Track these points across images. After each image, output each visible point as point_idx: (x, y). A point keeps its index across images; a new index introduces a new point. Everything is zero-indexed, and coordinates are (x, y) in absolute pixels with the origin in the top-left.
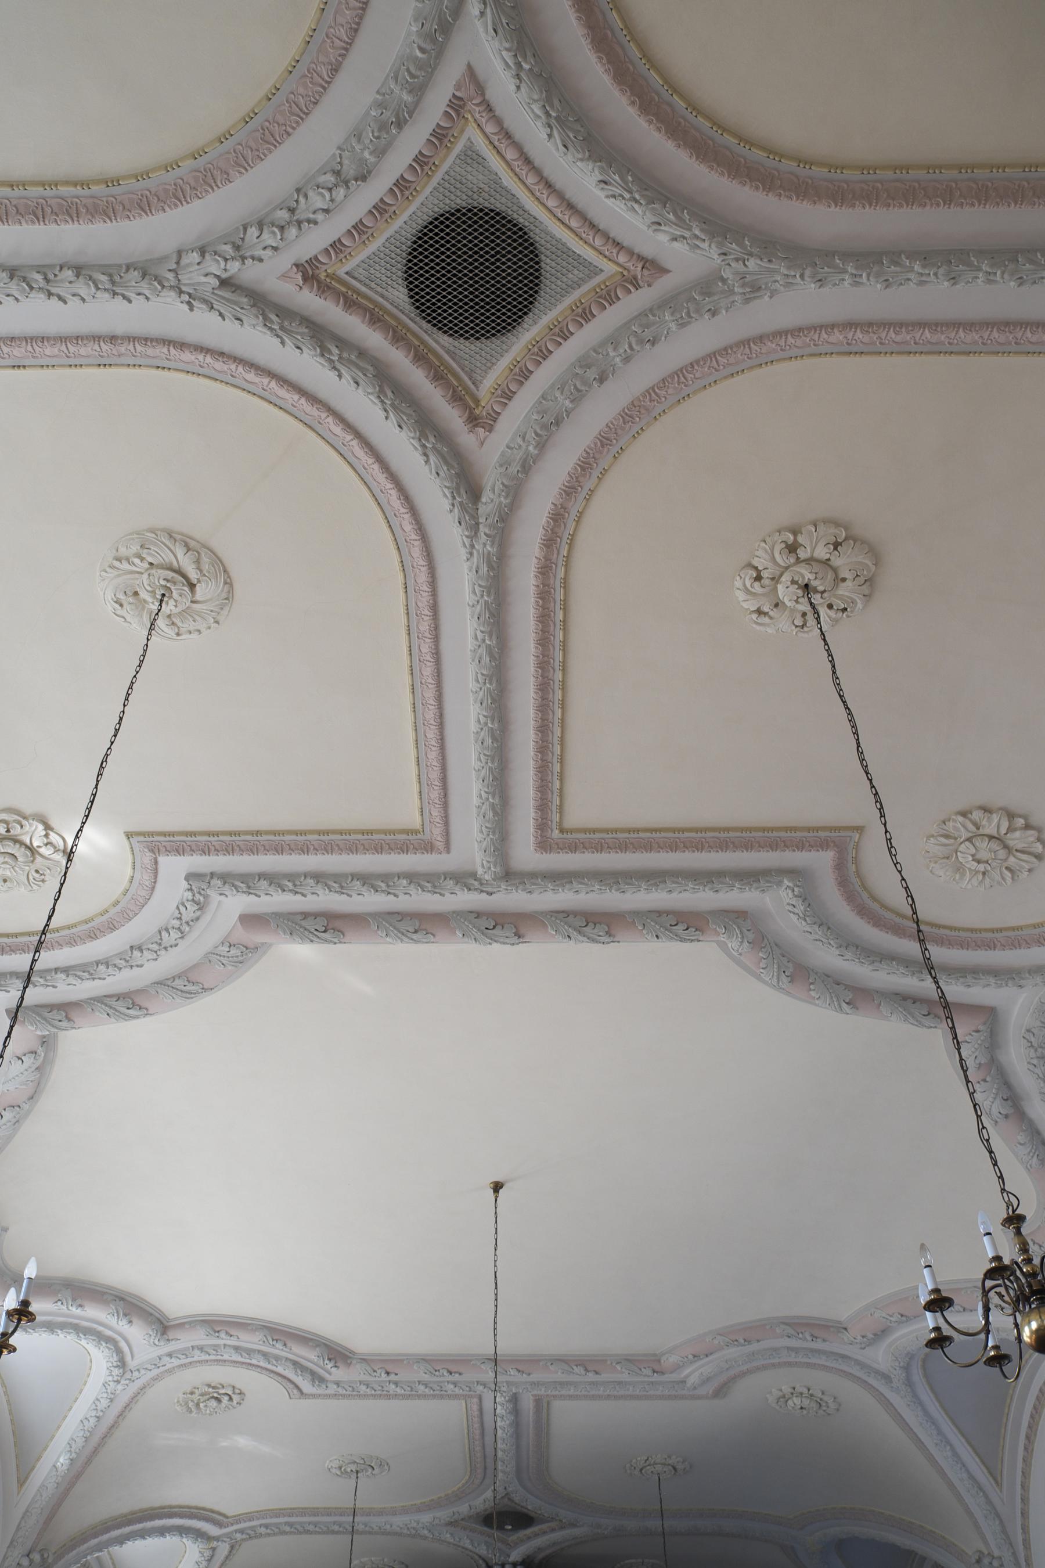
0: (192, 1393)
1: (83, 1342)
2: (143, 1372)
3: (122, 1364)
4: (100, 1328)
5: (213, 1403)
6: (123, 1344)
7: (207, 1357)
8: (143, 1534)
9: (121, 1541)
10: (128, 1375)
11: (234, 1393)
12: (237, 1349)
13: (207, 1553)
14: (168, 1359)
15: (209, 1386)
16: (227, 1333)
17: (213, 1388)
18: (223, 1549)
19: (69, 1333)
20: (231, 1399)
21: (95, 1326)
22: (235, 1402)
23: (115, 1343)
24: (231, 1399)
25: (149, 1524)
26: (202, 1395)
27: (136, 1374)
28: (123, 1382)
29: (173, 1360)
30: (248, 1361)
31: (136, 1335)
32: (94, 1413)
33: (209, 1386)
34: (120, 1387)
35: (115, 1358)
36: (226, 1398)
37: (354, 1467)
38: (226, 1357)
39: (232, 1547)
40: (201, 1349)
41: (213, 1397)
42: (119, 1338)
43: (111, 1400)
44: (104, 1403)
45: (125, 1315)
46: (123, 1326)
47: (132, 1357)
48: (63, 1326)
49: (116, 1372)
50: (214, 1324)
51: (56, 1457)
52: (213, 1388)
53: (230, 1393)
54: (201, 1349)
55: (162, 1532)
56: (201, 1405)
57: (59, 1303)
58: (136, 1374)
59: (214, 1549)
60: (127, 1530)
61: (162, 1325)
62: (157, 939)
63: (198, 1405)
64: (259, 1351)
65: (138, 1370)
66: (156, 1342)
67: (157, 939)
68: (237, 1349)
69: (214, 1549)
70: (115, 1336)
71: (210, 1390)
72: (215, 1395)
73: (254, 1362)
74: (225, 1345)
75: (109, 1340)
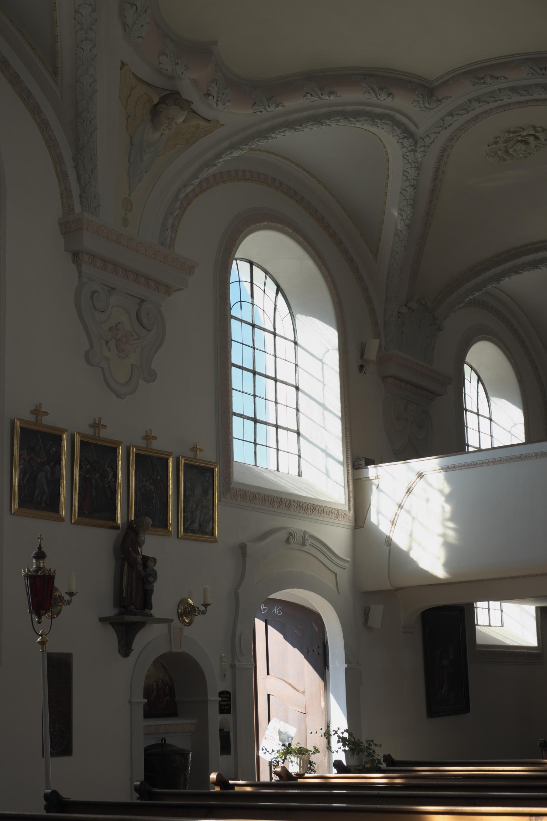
0: (496, 143)
1: (358, 125)
2: (433, 136)
3: (407, 134)
4: (368, 108)
6: (399, 117)
7: (486, 107)
8: (517, 270)
9: (497, 278)
11: (536, 131)
12: (513, 89)
14: (450, 118)
15: (509, 132)
16: (492, 77)
17: (514, 132)
19: (339, 120)
20: (537, 138)
21: (362, 108)
22: (543, 140)
23: (392, 119)
24: (537, 138)
25: (519, 261)
26: (506, 141)
27: (427, 140)
28: (419, 150)
29: (455, 118)
30: (529, 97)
31: (402, 103)
32: (407, 183)
33: (509, 132)
34: (419, 155)
35: (399, 131)
36: (531, 139)
38: (506, 101)
40: (478, 100)
41: (518, 141)
42: (392, 113)
43: (418, 168)
45: (381, 89)
46: (384, 100)
47: (417, 126)
48: (329, 116)
49: (406, 143)
50: (475, 72)
51: (395, 215)
52: (514, 132)
53: (533, 133)
54: (478, 100)
55: (535, 265)
56: (511, 151)
57: (309, 96)
58: (427, 140)
60: (499, 269)
61: (427, 90)
62: (405, 178)
63: (507, 152)
64: (536, 85)
65: (428, 136)
66: (428, 106)
67: (405, 178)
68: (513, 89)
70: (387, 112)
71: (511, 135)
72: (519, 138)
73: (536, 96)
74: (500, 90)
75: (381, 117)
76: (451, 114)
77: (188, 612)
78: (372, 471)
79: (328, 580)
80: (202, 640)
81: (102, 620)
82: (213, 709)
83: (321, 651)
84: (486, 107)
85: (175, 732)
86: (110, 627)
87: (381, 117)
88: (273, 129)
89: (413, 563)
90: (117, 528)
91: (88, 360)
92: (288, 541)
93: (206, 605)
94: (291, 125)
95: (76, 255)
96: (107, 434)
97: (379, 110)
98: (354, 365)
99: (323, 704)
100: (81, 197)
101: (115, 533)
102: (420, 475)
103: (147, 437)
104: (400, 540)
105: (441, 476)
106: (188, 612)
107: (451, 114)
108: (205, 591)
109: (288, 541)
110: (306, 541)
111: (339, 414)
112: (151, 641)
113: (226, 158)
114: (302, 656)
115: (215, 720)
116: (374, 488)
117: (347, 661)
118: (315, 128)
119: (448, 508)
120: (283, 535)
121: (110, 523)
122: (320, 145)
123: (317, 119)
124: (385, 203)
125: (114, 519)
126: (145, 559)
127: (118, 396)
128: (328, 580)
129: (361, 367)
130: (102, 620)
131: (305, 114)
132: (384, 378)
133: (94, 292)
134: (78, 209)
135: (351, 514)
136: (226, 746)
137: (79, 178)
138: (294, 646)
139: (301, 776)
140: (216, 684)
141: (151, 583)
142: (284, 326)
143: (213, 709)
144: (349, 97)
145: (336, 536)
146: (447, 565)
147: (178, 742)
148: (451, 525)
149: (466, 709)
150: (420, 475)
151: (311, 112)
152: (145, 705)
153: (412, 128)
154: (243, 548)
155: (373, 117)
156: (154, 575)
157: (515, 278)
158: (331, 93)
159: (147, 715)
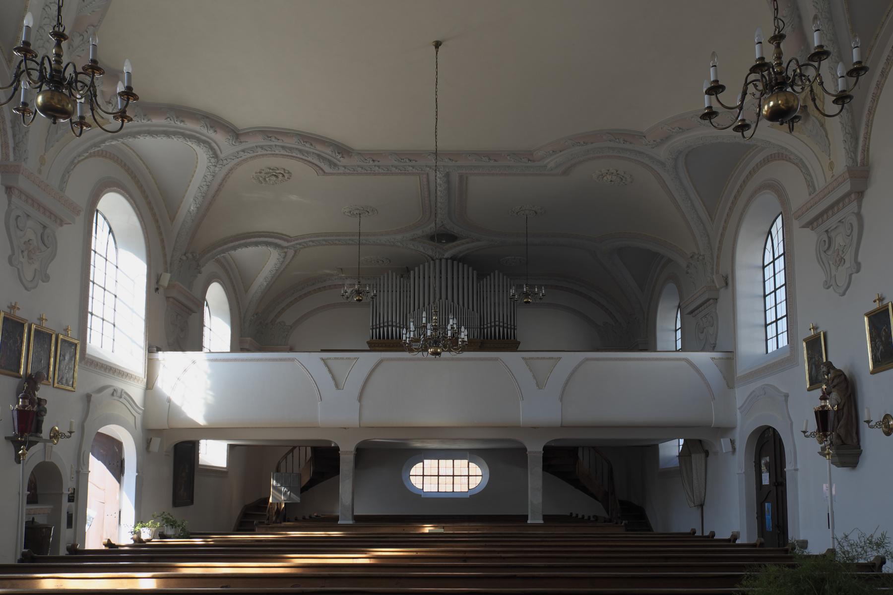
1: (189, 143)
3: (216, 156)
4: (198, 135)
5: (274, 178)
6: (214, 145)
7: (265, 152)
8: (246, 245)
9: (235, 248)
10: (221, 162)
12: (283, 147)
13: (283, 254)
18: (291, 253)
20: (283, 176)
23: (209, 144)
24: (283, 176)
31: (220, 138)
34: (217, 169)
37: (358, 212)
39: (296, 252)
40: (262, 147)
43: (214, 176)
44: (210, 178)
45: (211, 127)
46: (211, 133)
48: (175, 134)
49: (213, 160)
50: (267, 133)
54: (262, 147)
55: (256, 244)
58: (225, 162)
59: (286, 253)
61: (236, 134)
63: (265, 179)
68: (283, 147)
69: (286, 253)
73: (294, 154)
75: (204, 142)
76: (243, 151)
77: (56, 435)
78: (160, 355)
79: (131, 420)
80: (62, 454)
81: (6, 438)
82: (65, 499)
83: (119, 464)
84: (265, 152)
85: (41, 514)
86: (11, 443)
87: (204, 142)
88: (140, 133)
89: (183, 413)
90: (19, 377)
91: (10, 262)
92: (113, 394)
93: (71, 432)
94: (151, 133)
95: (9, 189)
96: (20, 314)
97: (204, 138)
98: (154, 286)
99: (118, 498)
100: (14, 149)
101: (18, 380)
102: (194, 362)
103: (41, 319)
104: (176, 400)
105: (207, 364)
106: (56, 435)
107: (243, 151)
108: (71, 423)
109: (113, 394)
110: (116, 393)
111: (144, 317)
112: (34, 455)
113: (107, 144)
114: (105, 467)
115: (65, 505)
116: (161, 366)
117: (137, 472)
118: (165, 139)
119: (209, 382)
120: (110, 390)
121: (16, 374)
122: (157, 148)
123: (167, 134)
124: (186, 191)
125: (18, 372)
126: (40, 400)
127: (26, 289)
128: (131, 420)
129: (157, 289)
130: (6, 438)
131: (161, 129)
132: (168, 298)
133: (18, 216)
134: (12, 158)
135: (145, 380)
136: (70, 525)
137: (14, 136)
138: (99, 459)
139: (149, 541)
140: (68, 485)
141: (43, 416)
142: (111, 256)
143: (65, 499)
144: (190, 126)
145: (136, 391)
146: (206, 417)
147: (40, 520)
148: (211, 393)
149: (192, 503)
150: (194, 362)
151: (165, 129)
152: (28, 496)
153: (219, 152)
154: (88, 397)
155: (199, 141)
156: (45, 411)
157: (245, 250)
158: (182, 121)
159: (29, 502)
